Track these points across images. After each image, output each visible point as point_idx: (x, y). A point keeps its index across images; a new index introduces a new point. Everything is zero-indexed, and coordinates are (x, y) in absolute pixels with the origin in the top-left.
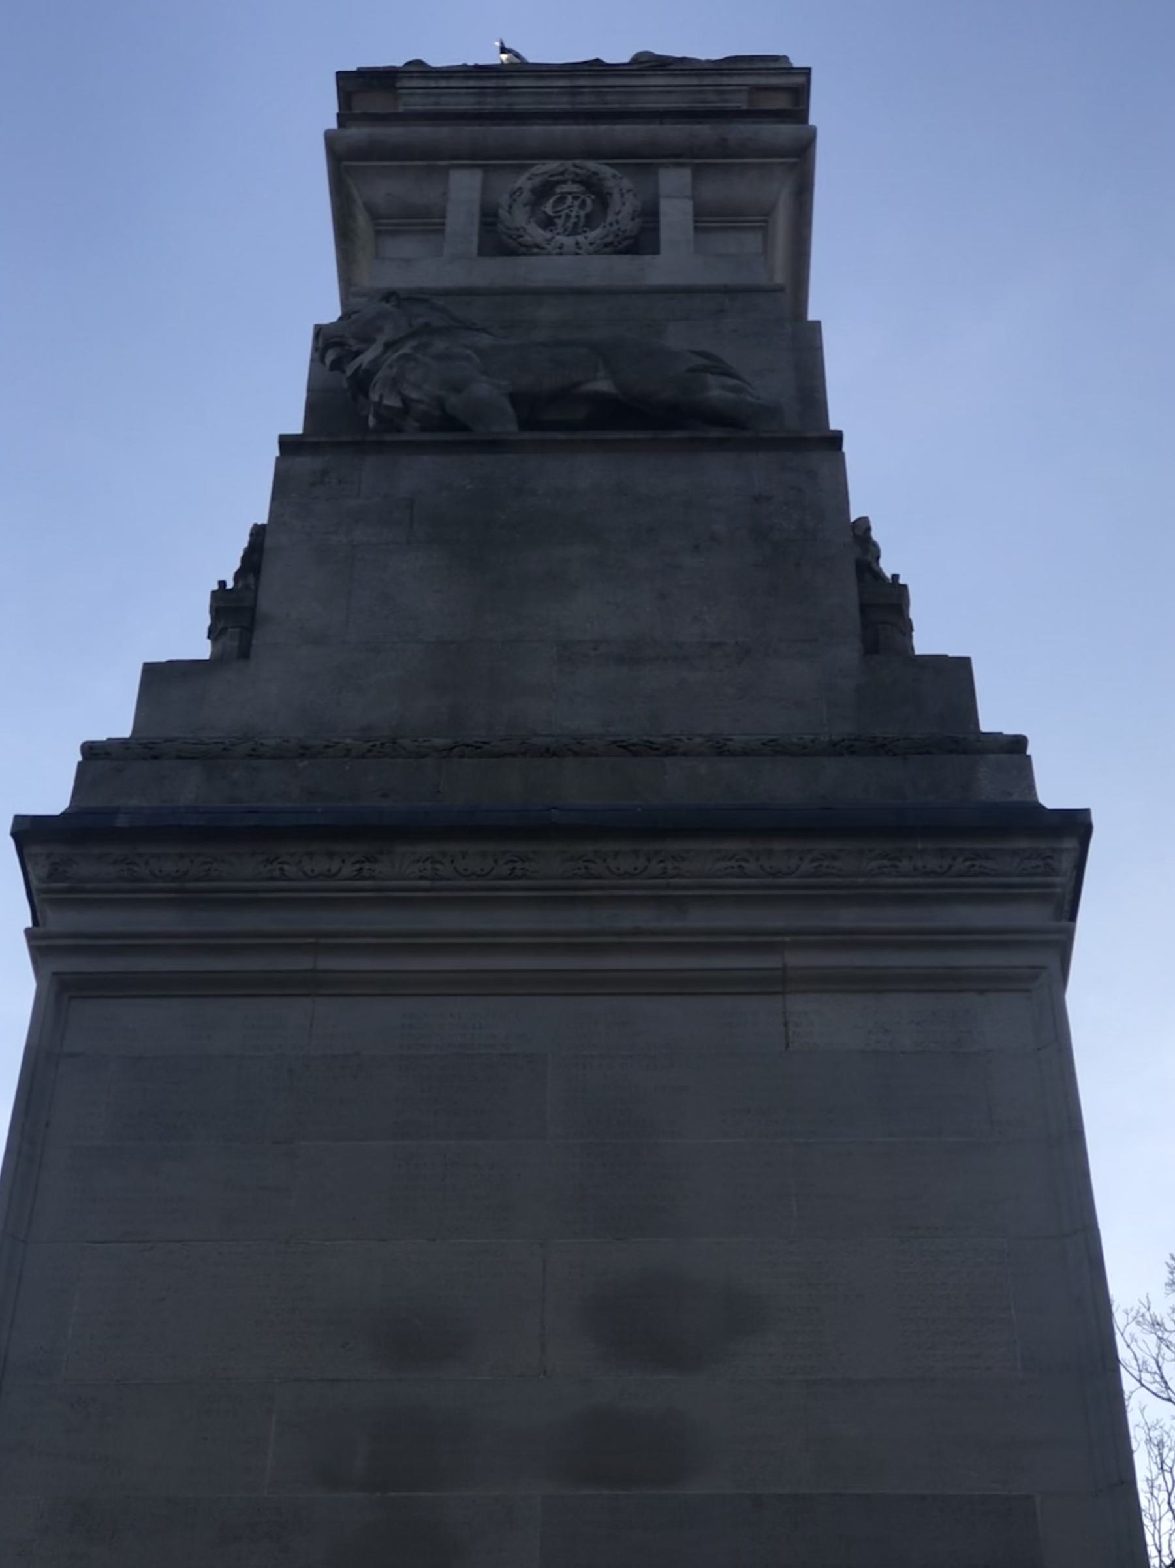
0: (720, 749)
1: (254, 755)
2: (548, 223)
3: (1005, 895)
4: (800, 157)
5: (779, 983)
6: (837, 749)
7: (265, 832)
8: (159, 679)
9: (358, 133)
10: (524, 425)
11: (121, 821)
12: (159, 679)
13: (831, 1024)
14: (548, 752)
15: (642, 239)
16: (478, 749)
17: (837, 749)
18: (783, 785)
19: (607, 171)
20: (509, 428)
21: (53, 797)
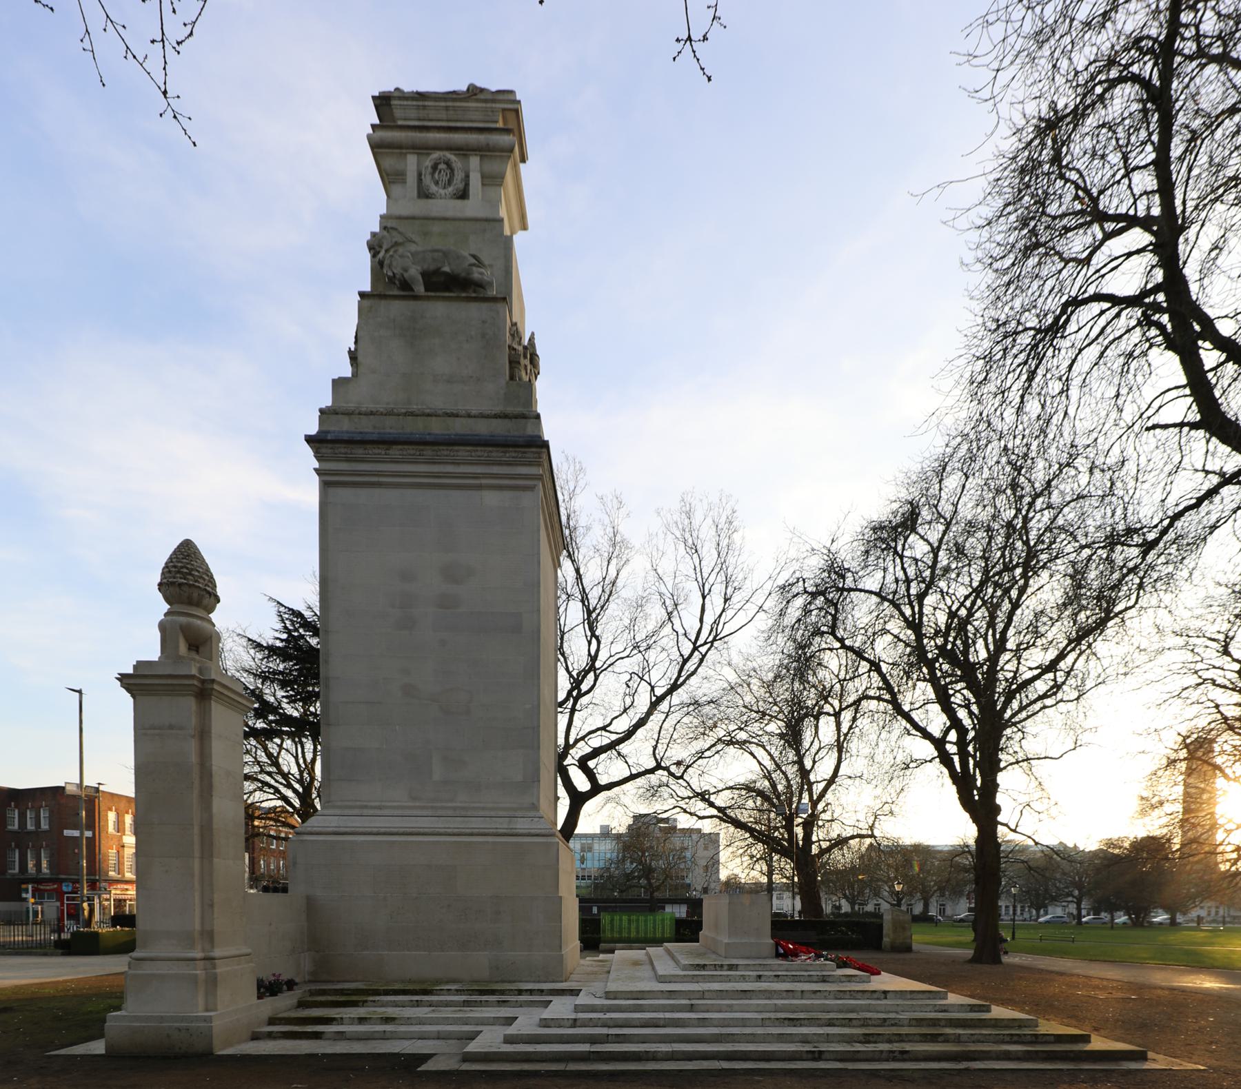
0: (469, 416)
1: (360, 414)
2: (437, 183)
3: (530, 464)
4: (167, 566)
5: (480, 487)
6: (496, 416)
7: (363, 442)
8: (338, 384)
9: (382, 134)
10: (426, 290)
11: (329, 437)
12: (338, 384)
13: (492, 499)
14: (429, 415)
15: (463, 195)
16: (412, 414)
17: (496, 416)
18: (483, 428)
19: (453, 158)
20: (420, 289)
21: (313, 429)
